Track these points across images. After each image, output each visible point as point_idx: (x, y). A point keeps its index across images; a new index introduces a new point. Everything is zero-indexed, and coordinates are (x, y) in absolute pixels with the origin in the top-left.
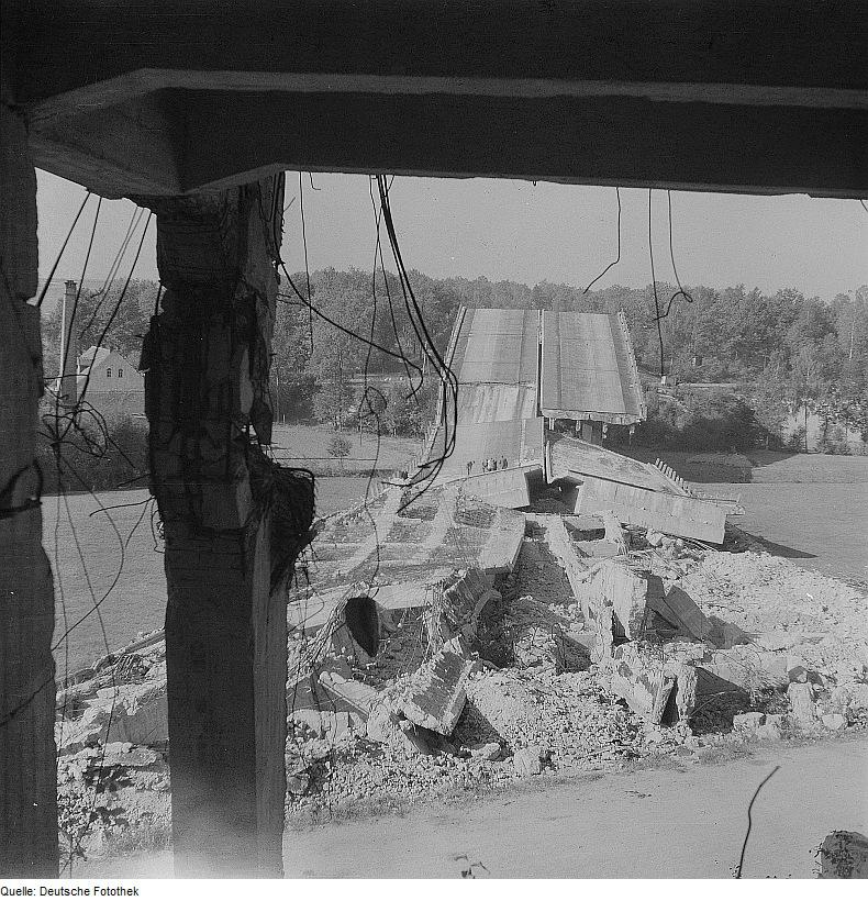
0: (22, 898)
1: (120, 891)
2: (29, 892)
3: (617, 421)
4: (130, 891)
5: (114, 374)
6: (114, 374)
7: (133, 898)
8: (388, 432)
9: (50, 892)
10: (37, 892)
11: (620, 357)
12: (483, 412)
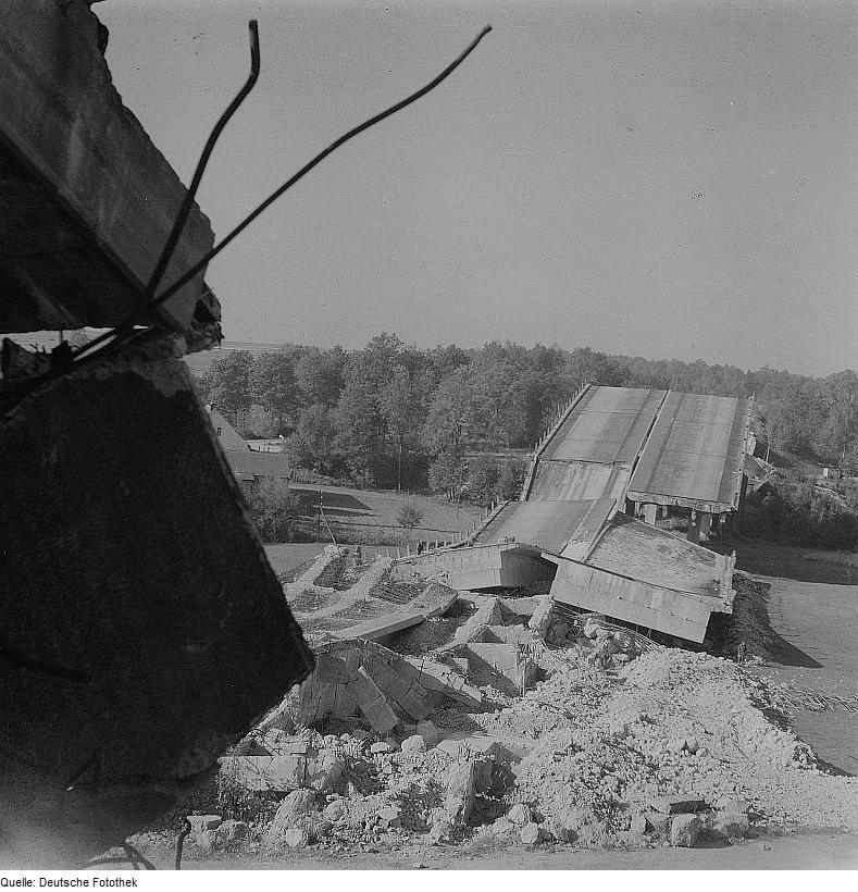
0: (22, 889)
1: (119, 882)
2: (28, 883)
3: (706, 508)
4: (128, 882)
7: (132, 889)
9: (50, 883)
10: (37, 883)
12: (571, 492)
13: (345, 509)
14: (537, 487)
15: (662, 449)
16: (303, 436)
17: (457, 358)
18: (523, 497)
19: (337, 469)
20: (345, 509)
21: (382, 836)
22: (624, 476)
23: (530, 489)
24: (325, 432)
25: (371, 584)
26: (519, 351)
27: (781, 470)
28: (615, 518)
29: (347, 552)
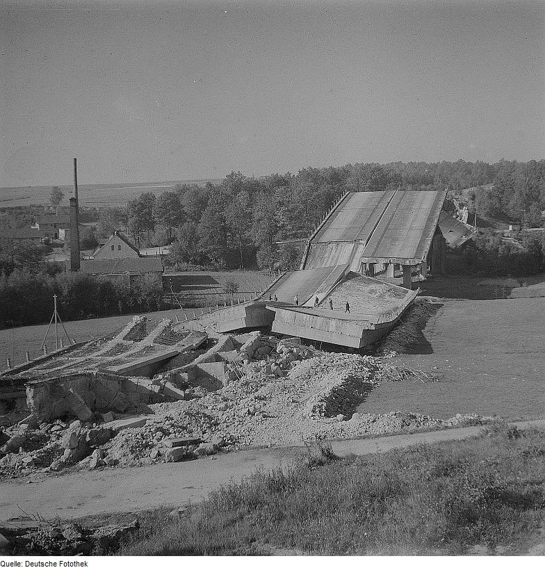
1: (76, 564)
2: (18, 564)
3: (407, 263)
4: (82, 563)
5: (116, 248)
6: (116, 248)
8: (397, 267)
9: (32, 564)
10: (23, 564)
11: (427, 227)
12: (330, 261)
13: (207, 286)
14: (310, 259)
15: (387, 228)
16: (182, 243)
17: (282, 182)
18: (301, 268)
19: (203, 260)
20: (207, 286)
21: (23, 471)
22: (361, 248)
23: (306, 262)
24: (193, 238)
25: (155, 336)
26: (316, 172)
27: (482, 230)
28: (348, 275)
29: (145, 319)
